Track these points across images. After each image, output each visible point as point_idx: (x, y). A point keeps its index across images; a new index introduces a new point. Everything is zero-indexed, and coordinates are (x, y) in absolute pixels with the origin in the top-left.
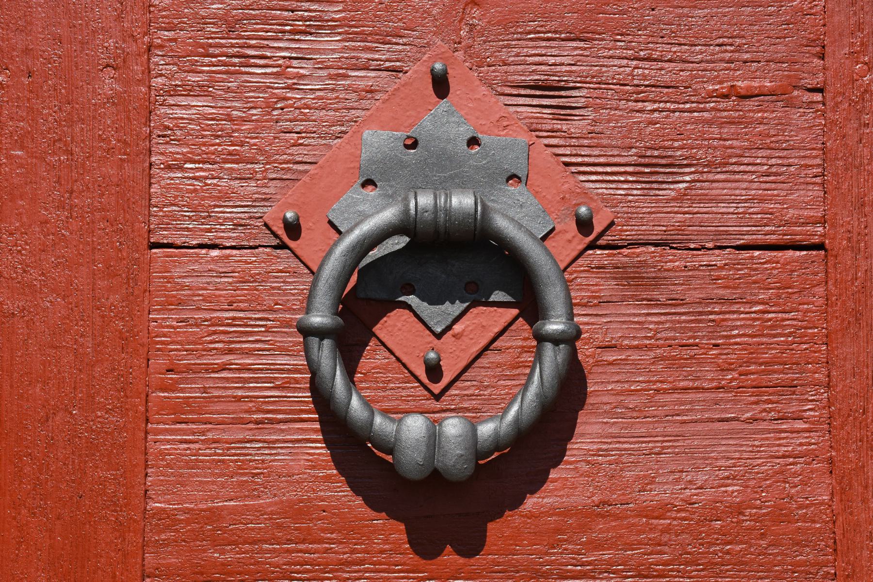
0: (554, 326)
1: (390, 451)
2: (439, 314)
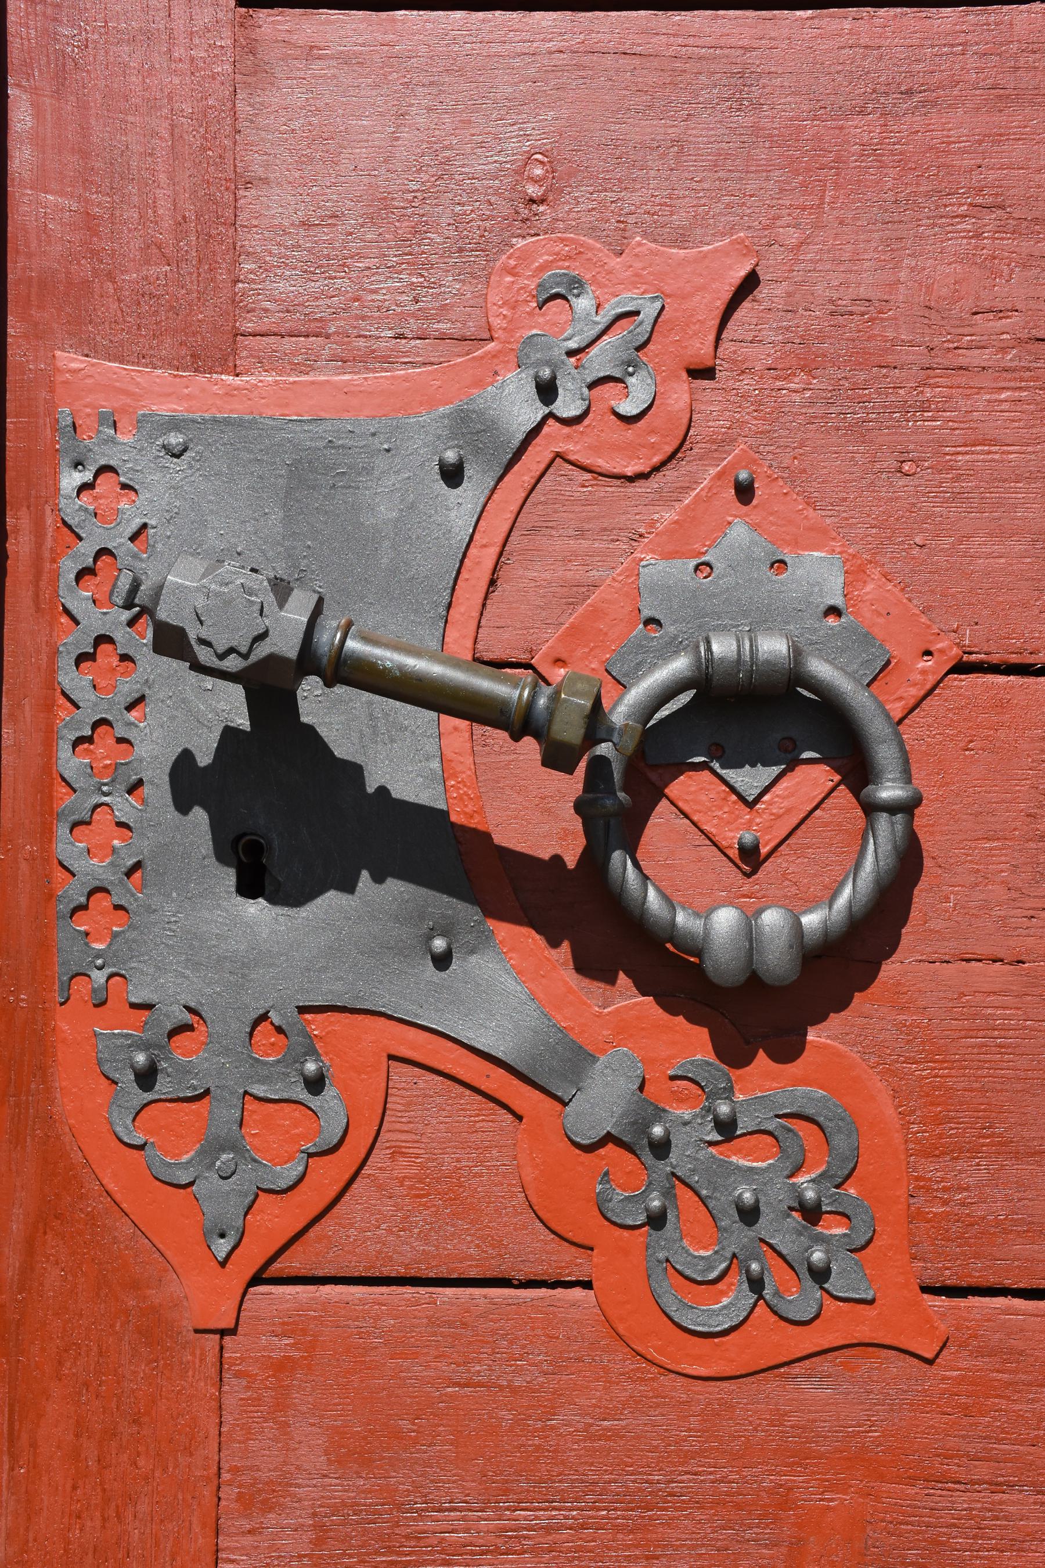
0: (889, 792)
1: (699, 953)
2: (749, 779)
